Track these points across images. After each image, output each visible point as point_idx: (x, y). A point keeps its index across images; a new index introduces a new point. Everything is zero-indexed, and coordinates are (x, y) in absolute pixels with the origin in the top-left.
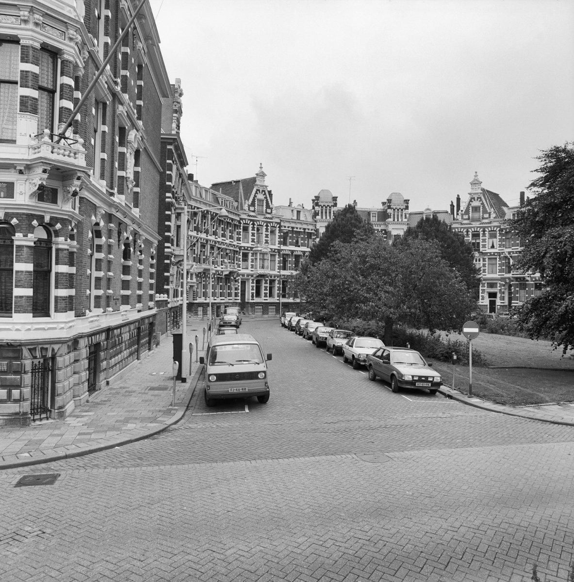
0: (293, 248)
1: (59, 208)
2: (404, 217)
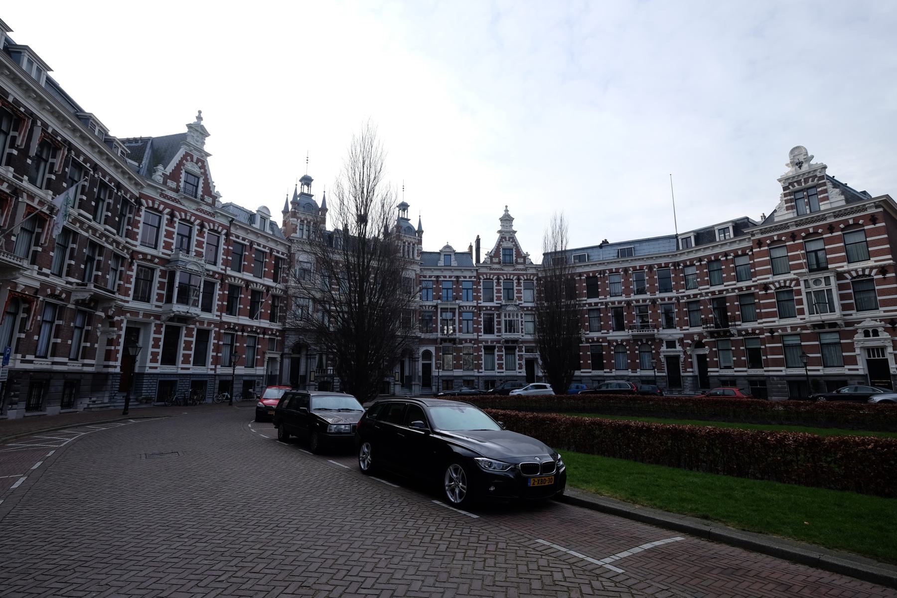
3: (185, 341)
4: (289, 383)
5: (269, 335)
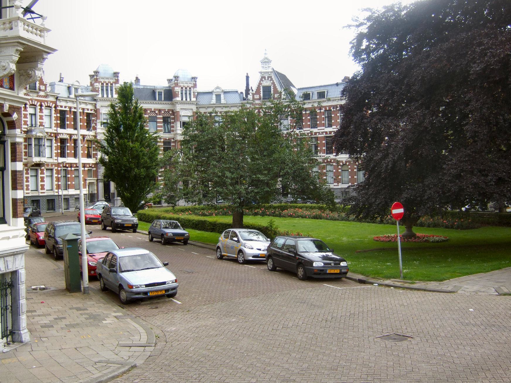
0: (71, 131)
1: (16, 95)
2: (192, 96)
3: (41, 177)
4: (104, 199)
5: (87, 167)
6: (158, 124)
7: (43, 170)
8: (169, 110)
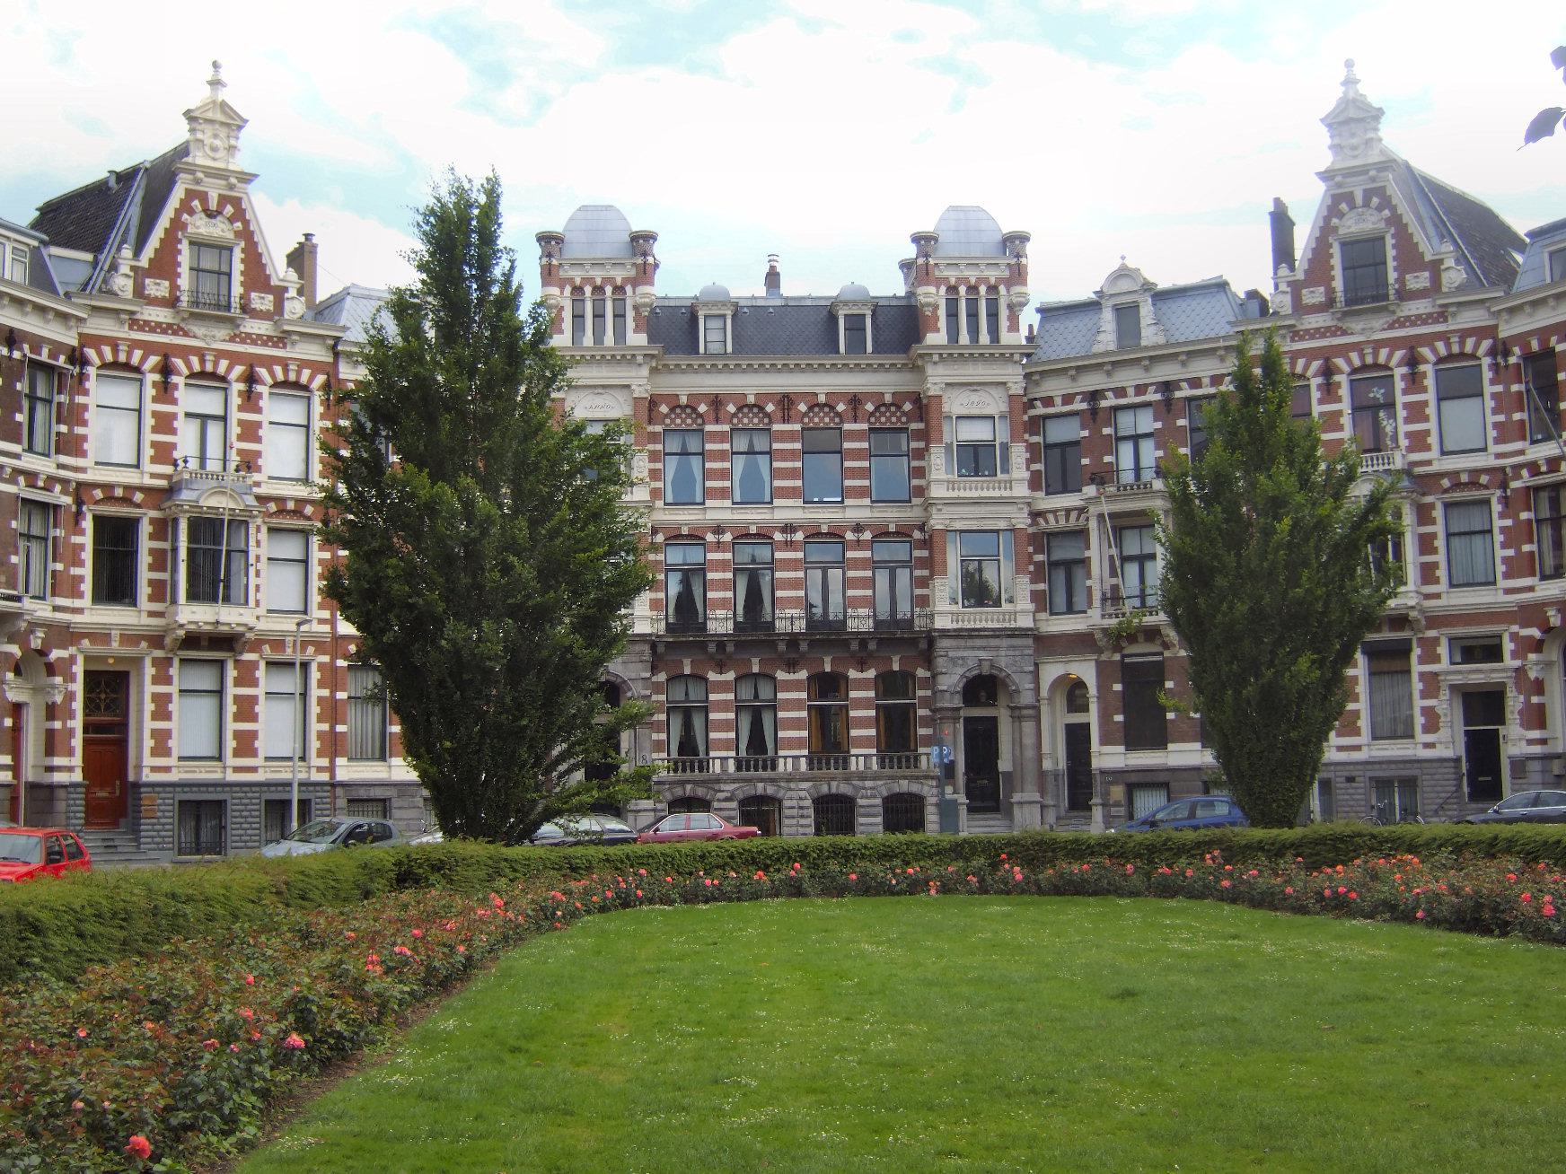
6: (847, 464)
7: (254, 665)
8: (898, 398)
